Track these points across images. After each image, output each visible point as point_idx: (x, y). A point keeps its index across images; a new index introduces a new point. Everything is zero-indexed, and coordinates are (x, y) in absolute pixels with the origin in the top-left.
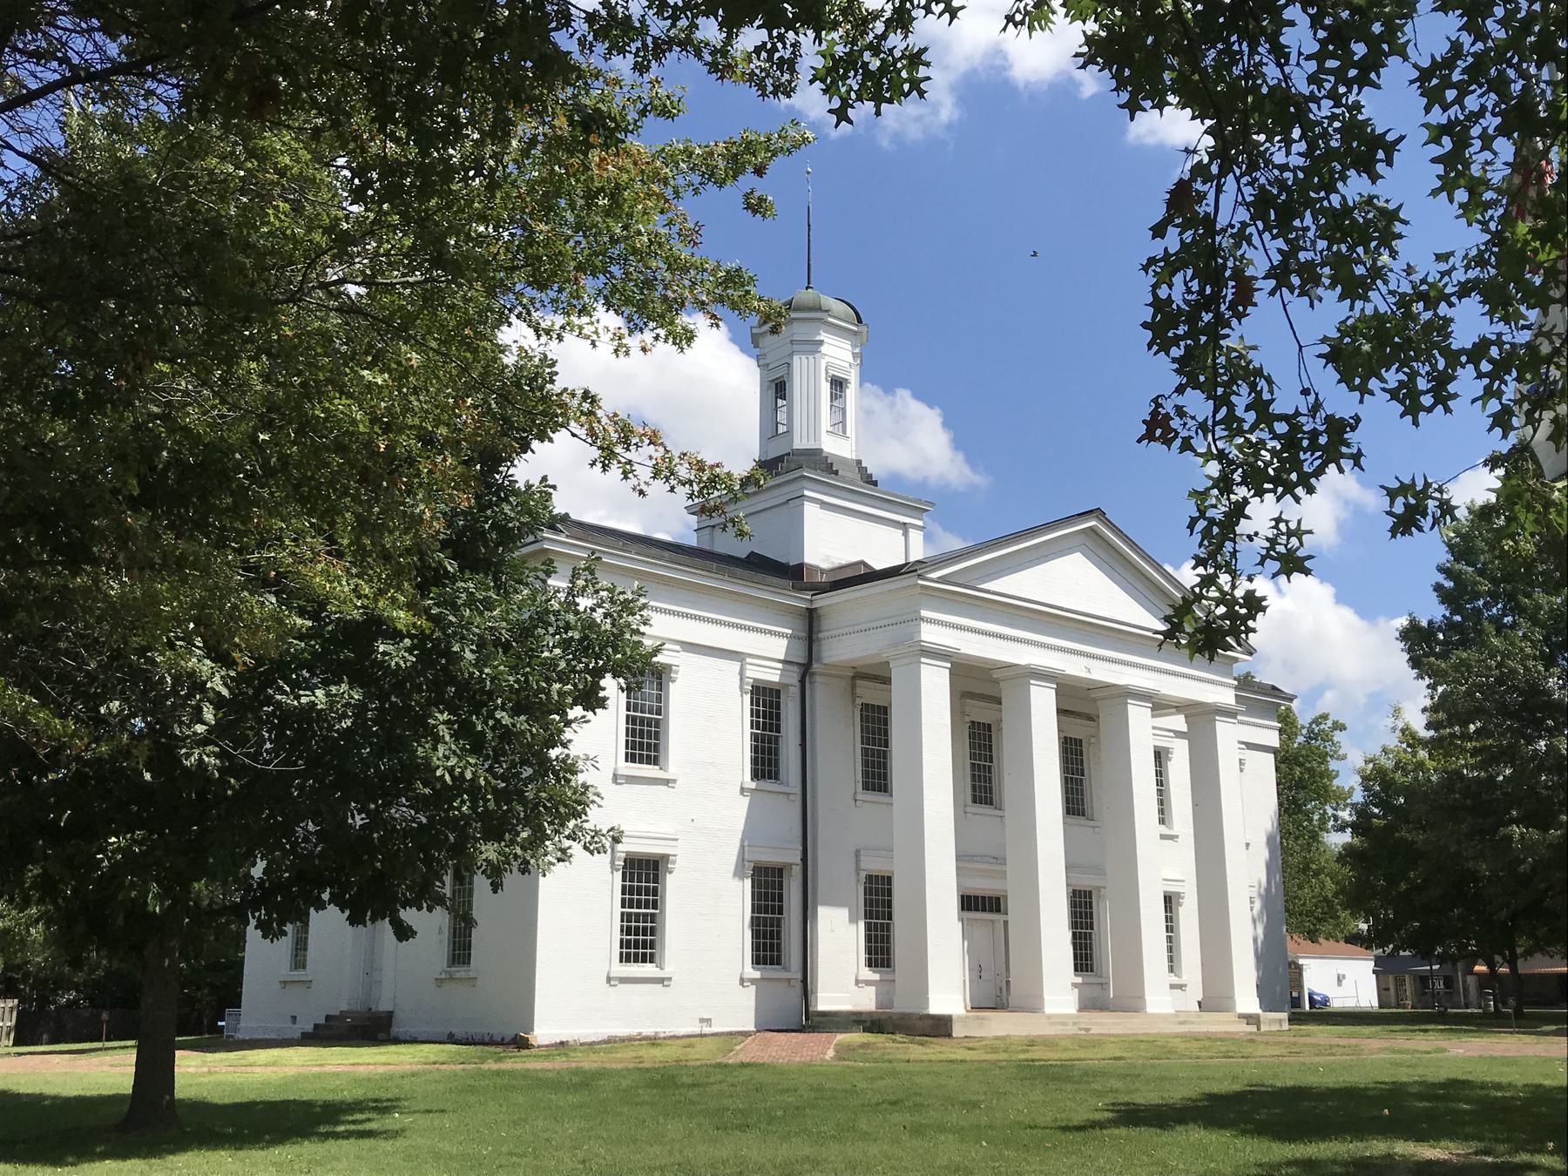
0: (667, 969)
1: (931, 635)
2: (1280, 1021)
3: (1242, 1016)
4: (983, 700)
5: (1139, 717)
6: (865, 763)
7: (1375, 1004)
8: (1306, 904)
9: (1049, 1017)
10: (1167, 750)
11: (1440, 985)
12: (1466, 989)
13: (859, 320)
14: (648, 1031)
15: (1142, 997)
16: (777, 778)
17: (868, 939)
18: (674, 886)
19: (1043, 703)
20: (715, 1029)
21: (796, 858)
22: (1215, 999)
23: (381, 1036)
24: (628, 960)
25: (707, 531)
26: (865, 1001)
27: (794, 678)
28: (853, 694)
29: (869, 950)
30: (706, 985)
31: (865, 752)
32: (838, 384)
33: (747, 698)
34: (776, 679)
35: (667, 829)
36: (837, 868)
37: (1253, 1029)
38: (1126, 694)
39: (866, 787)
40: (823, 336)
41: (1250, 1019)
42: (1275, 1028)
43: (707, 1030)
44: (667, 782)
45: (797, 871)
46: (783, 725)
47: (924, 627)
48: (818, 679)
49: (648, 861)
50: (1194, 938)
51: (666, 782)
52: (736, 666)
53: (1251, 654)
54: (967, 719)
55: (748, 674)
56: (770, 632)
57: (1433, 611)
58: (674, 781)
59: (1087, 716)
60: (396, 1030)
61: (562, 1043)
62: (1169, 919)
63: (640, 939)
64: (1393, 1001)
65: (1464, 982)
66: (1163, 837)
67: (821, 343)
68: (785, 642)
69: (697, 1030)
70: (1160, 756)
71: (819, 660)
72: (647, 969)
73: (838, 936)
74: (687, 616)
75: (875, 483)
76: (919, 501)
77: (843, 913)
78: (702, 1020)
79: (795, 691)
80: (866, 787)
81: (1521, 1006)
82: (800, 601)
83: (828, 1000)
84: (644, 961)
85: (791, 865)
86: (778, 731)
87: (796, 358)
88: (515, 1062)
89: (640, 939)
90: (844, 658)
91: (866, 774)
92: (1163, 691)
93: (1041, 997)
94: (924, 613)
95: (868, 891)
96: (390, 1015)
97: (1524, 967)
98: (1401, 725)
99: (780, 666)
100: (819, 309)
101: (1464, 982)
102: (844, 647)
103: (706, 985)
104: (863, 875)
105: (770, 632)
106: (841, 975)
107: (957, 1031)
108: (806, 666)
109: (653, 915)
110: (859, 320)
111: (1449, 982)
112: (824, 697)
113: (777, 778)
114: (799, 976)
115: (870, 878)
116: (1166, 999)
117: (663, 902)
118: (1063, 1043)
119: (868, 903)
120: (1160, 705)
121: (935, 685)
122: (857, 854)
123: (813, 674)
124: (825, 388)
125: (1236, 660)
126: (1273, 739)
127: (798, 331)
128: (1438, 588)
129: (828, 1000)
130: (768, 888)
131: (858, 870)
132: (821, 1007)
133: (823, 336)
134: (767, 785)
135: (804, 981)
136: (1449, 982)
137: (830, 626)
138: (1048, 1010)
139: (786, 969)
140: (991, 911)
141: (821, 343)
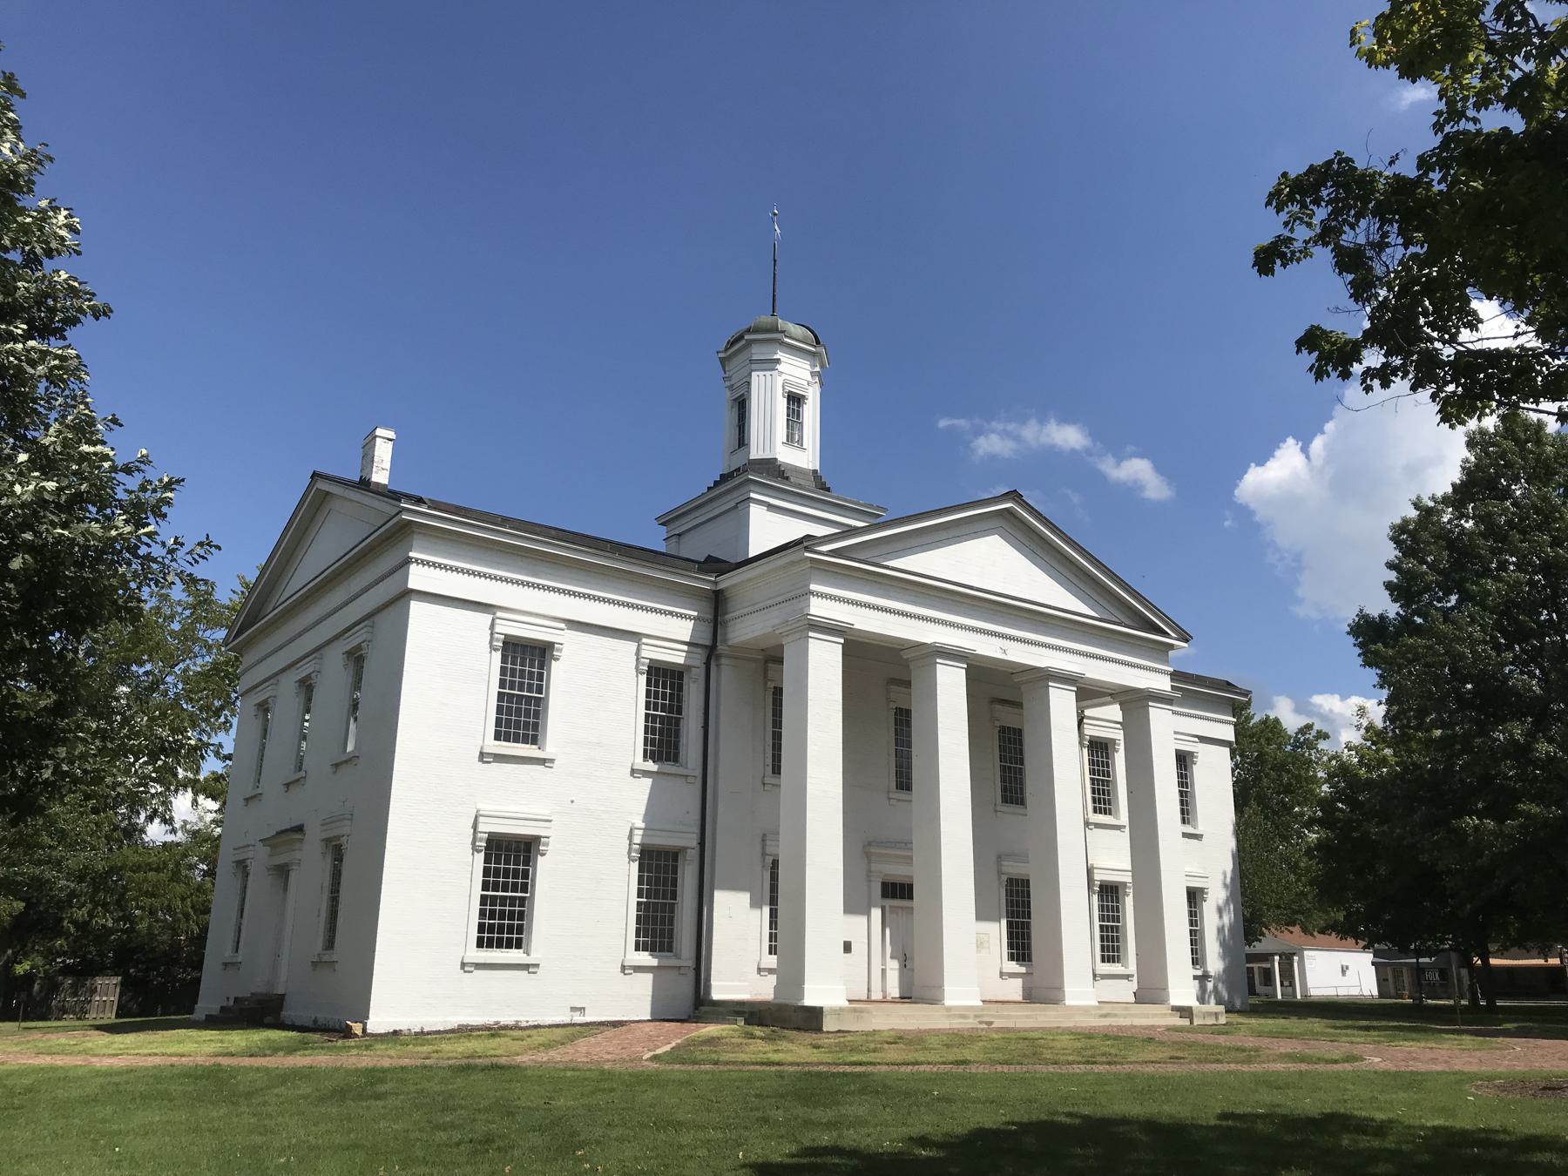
0: (533, 955)
1: (819, 608)
2: (1216, 1015)
3: (1175, 1009)
4: (885, 685)
5: (1062, 702)
6: (1003, 780)
7: (1375, 993)
8: (1271, 899)
9: (949, 1009)
10: (1191, 754)
11: (1434, 977)
12: (1460, 980)
13: (818, 342)
14: (489, 1019)
15: (1060, 988)
16: (676, 760)
17: (1010, 935)
18: (545, 869)
19: (951, 685)
20: (588, 1019)
21: (692, 841)
22: (1150, 991)
23: (268, 1020)
24: (490, 945)
25: (674, 540)
26: (763, 990)
27: (699, 660)
28: (765, 676)
29: (1010, 946)
30: (585, 970)
31: (1003, 769)
32: (795, 400)
33: (498, 656)
34: (681, 661)
35: (541, 810)
36: (728, 846)
37: (1186, 1022)
38: (1045, 677)
39: (1005, 800)
40: (780, 355)
41: (1185, 1012)
42: (1211, 1021)
43: (578, 1019)
44: (542, 762)
45: (693, 855)
46: (684, 706)
47: (813, 600)
48: (723, 661)
49: (667, 853)
50: (1131, 930)
51: (542, 762)
52: (633, 646)
53: (1186, 641)
54: (893, 705)
55: (644, 654)
56: (671, 613)
57: (1385, 606)
58: (552, 761)
59: (1005, 703)
60: (287, 1014)
61: (395, 1032)
62: (1191, 914)
63: (504, 921)
64: (1392, 991)
65: (1459, 974)
66: (1185, 835)
67: (778, 361)
68: (690, 624)
69: (567, 1020)
70: (1184, 761)
71: (725, 641)
72: (513, 955)
73: (736, 922)
74: (549, 589)
75: (828, 490)
76: (870, 506)
77: (744, 898)
78: (573, 1009)
79: (699, 673)
80: (1005, 800)
81: (1492, 1007)
82: (704, 583)
83: (722, 989)
84: (509, 946)
85: (684, 849)
86: (680, 712)
87: (754, 374)
88: (321, 1058)
89: (504, 921)
90: (743, 638)
91: (1004, 789)
92: (1088, 675)
93: (940, 987)
94: (813, 587)
95: (1009, 893)
96: (282, 997)
97: (1493, 961)
98: (1365, 723)
99: (685, 648)
100: (775, 330)
101: (1459, 974)
102: (746, 629)
103: (585, 970)
104: (1004, 878)
105: (671, 613)
106: (739, 965)
107: (829, 1024)
108: (710, 648)
109: (523, 899)
110: (818, 342)
111: (1444, 974)
112: (726, 677)
113: (676, 760)
114: (691, 963)
115: (1010, 881)
116: (1089, 990)
117: (533, 886)
118: (933, 1041)
119: (1010, 903)
120: (1089, 693)
121: (823, 667)
122: (999, 857)
123: (718, 657)
124: (782, 405)
125: (1172, 647)
126: (1228, 733)
127: (758, 352)
128: (1389, 586)
129: (722, 989)
130: (657, 867)
131: (1000, 873)
132: (716, 995)
133: (780, 355)
134: (669, 767)
135: (697, 969)
136: (1444, 974)
137: (736, 609)
138: (948, 1002)
139: (678, 957)
140: (902, 897)
141: (778, 361)
